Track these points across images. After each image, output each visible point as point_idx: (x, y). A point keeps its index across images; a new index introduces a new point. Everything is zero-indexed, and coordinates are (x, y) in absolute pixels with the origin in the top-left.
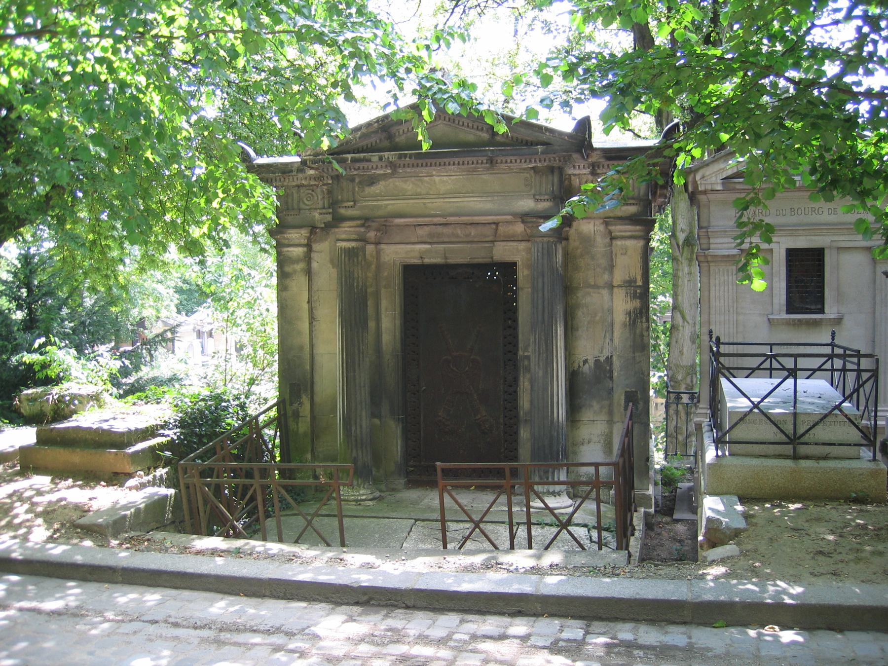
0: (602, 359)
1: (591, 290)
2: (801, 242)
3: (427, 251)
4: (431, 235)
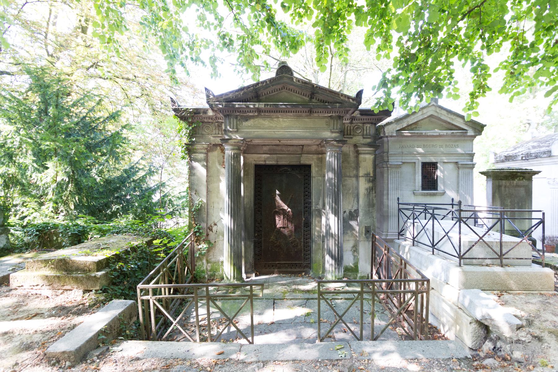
0: (353, 211)
1: (347, 178)
2: (427, 160)
3: (268, 158)
4: (270, 150)
